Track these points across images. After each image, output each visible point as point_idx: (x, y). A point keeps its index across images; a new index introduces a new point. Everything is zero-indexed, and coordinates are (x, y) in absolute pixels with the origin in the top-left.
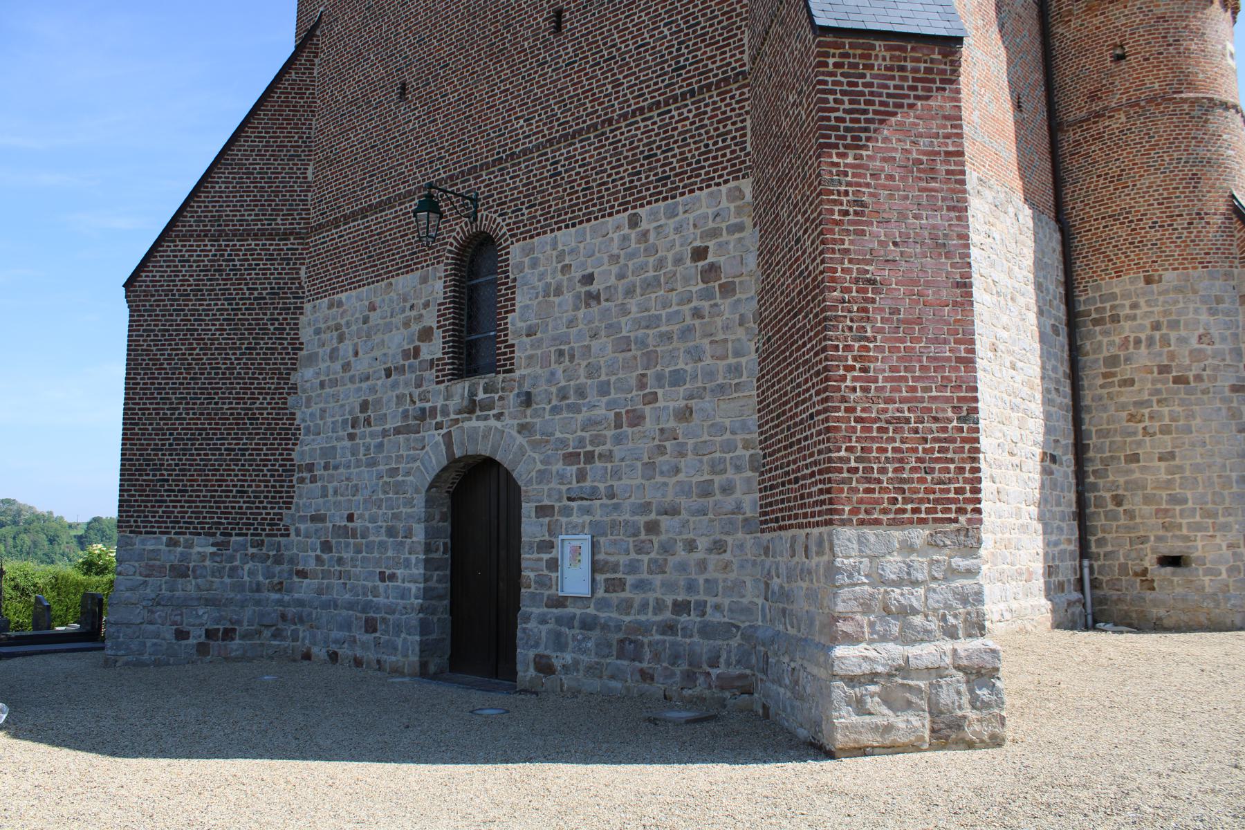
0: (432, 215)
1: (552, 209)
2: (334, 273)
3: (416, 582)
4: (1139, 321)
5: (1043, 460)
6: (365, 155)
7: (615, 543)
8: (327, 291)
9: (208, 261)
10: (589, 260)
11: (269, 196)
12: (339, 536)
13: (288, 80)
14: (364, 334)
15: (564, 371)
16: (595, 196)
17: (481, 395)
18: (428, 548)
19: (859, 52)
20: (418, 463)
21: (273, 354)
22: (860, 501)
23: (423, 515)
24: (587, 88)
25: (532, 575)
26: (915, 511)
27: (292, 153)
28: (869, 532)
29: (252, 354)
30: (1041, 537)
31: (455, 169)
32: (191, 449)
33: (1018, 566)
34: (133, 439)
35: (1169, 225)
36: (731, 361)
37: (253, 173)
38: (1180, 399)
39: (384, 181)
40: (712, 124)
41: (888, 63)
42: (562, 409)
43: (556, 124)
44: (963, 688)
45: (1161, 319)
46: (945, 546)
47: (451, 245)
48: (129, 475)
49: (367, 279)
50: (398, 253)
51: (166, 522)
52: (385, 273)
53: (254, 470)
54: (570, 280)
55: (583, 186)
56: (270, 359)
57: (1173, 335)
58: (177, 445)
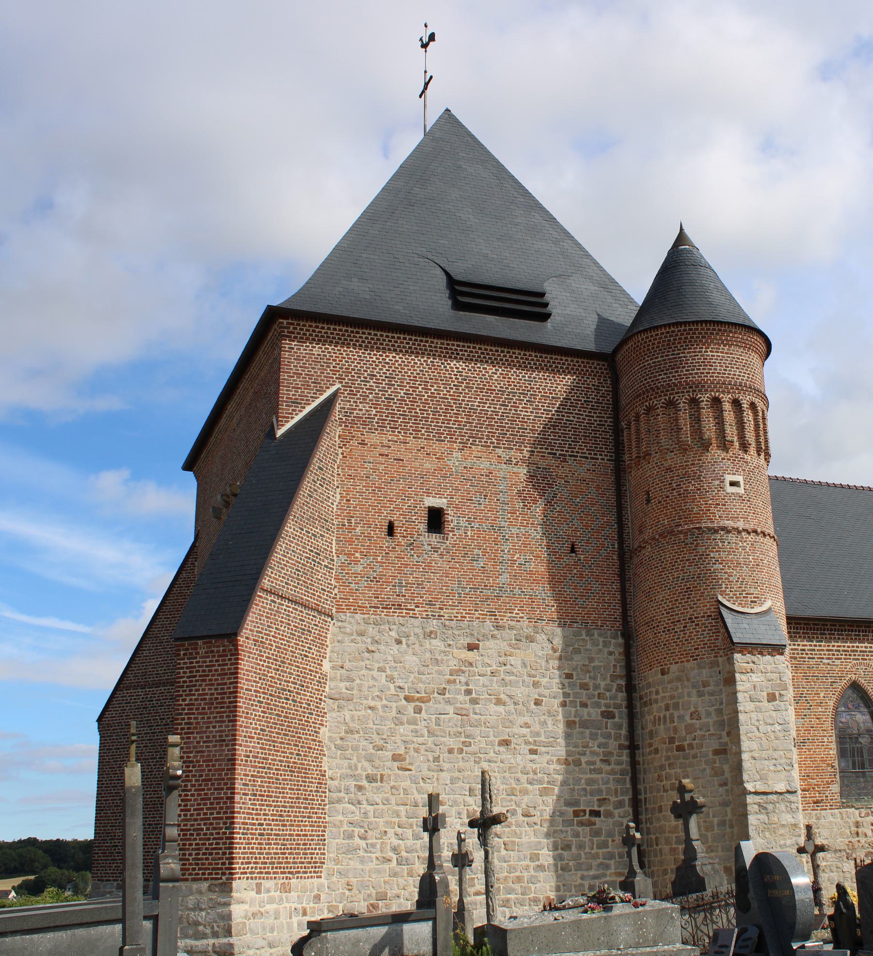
26: (203, 874)
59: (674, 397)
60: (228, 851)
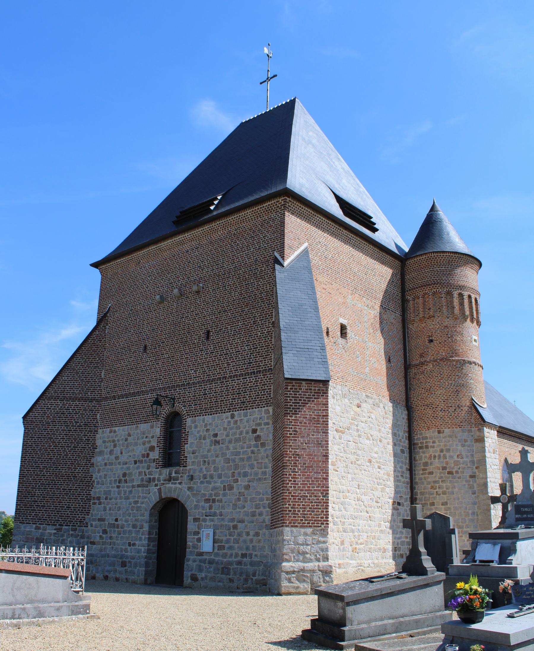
0: (158, 407)
1: (203, 407)
2: (113, 419)
3: (144, 546)
4: (435, 449)
5: (393, 504)
6: (128, 372)
7: (221, 532)
8: (109, 425)
9: (59, 409)
10: (216, 428)
11: (85, 383)
12: (111, 528)
13: (95, 334)
14: (125, 445)
15: (206, 468)
16: (219, 405)
17: (174, 475)
18: (150, 533)
19: (298, 385)
20: (147, 499)
21: (84, 450)
22: (292, 520)
23: (148, 520)
24: (217, 363)
25: (191, 544)
26: (308, 523)
27: (96, 365)
28: (293, 529)
29: (75, 449)
30: (391, 535)
31: (166, 385)
32: (48, 489)
33: (379, 546)
34: (23, 483)
35: (447, 410)
36: (263, 470)
37: (79, 373)
38: (450, 481)
39: (136, 384)
40: (260, 385)
41: (306, 388)
42: (204, 483)
43: (206, 375)
44: (321, 576)
45: (444, 448)
46: (317, 534)
47: (164, 415)
48: (20, 498)
49: (127, 423)
50: (141, 415)
51: (35, 519)
52: (136, 422)
53: (74, 498)
54: (209, 435)
55: (215, 400)
56: (83, 452)
57: (448, 455)
58: (42, 486)
59: (451, 290)
60: (325, 510)
